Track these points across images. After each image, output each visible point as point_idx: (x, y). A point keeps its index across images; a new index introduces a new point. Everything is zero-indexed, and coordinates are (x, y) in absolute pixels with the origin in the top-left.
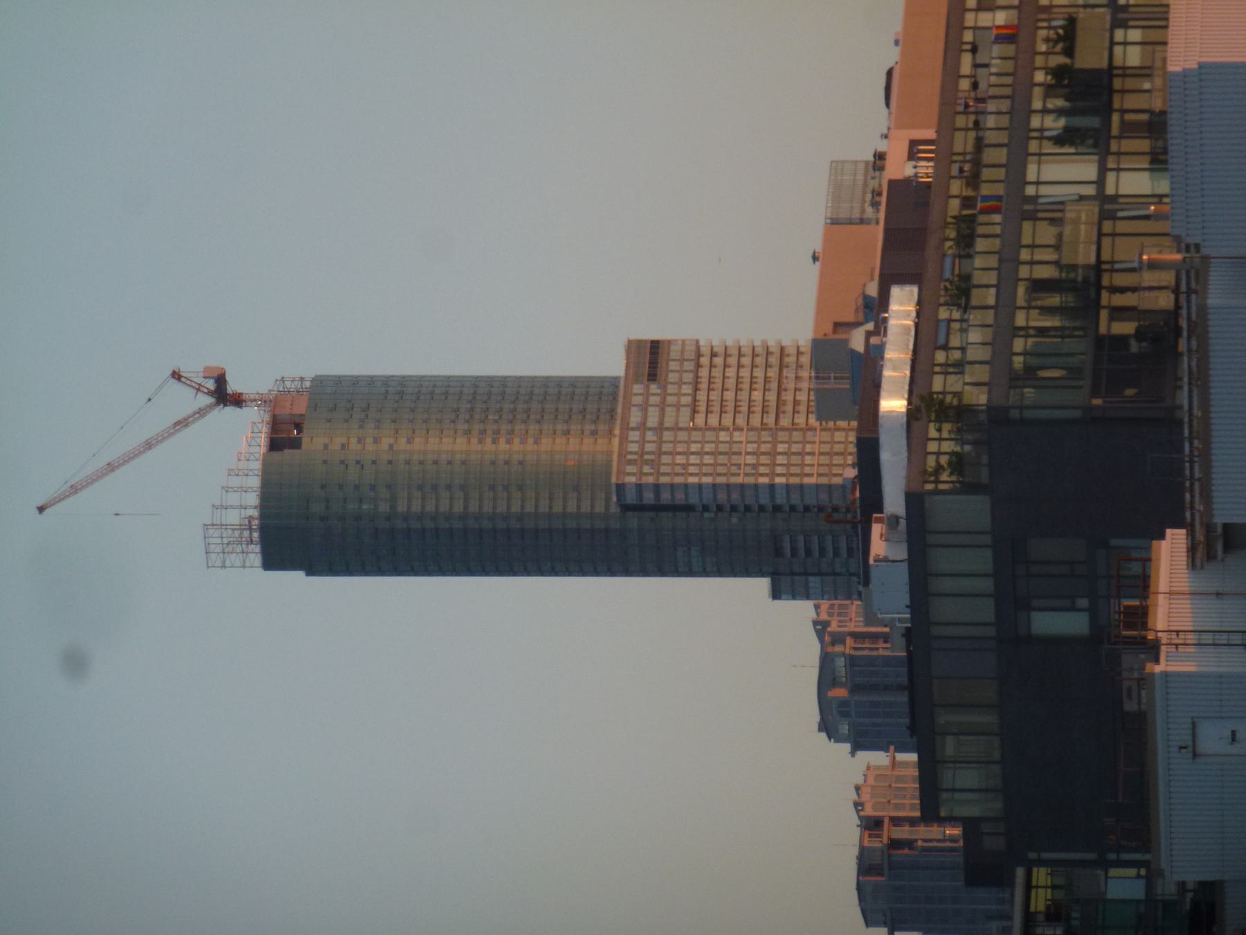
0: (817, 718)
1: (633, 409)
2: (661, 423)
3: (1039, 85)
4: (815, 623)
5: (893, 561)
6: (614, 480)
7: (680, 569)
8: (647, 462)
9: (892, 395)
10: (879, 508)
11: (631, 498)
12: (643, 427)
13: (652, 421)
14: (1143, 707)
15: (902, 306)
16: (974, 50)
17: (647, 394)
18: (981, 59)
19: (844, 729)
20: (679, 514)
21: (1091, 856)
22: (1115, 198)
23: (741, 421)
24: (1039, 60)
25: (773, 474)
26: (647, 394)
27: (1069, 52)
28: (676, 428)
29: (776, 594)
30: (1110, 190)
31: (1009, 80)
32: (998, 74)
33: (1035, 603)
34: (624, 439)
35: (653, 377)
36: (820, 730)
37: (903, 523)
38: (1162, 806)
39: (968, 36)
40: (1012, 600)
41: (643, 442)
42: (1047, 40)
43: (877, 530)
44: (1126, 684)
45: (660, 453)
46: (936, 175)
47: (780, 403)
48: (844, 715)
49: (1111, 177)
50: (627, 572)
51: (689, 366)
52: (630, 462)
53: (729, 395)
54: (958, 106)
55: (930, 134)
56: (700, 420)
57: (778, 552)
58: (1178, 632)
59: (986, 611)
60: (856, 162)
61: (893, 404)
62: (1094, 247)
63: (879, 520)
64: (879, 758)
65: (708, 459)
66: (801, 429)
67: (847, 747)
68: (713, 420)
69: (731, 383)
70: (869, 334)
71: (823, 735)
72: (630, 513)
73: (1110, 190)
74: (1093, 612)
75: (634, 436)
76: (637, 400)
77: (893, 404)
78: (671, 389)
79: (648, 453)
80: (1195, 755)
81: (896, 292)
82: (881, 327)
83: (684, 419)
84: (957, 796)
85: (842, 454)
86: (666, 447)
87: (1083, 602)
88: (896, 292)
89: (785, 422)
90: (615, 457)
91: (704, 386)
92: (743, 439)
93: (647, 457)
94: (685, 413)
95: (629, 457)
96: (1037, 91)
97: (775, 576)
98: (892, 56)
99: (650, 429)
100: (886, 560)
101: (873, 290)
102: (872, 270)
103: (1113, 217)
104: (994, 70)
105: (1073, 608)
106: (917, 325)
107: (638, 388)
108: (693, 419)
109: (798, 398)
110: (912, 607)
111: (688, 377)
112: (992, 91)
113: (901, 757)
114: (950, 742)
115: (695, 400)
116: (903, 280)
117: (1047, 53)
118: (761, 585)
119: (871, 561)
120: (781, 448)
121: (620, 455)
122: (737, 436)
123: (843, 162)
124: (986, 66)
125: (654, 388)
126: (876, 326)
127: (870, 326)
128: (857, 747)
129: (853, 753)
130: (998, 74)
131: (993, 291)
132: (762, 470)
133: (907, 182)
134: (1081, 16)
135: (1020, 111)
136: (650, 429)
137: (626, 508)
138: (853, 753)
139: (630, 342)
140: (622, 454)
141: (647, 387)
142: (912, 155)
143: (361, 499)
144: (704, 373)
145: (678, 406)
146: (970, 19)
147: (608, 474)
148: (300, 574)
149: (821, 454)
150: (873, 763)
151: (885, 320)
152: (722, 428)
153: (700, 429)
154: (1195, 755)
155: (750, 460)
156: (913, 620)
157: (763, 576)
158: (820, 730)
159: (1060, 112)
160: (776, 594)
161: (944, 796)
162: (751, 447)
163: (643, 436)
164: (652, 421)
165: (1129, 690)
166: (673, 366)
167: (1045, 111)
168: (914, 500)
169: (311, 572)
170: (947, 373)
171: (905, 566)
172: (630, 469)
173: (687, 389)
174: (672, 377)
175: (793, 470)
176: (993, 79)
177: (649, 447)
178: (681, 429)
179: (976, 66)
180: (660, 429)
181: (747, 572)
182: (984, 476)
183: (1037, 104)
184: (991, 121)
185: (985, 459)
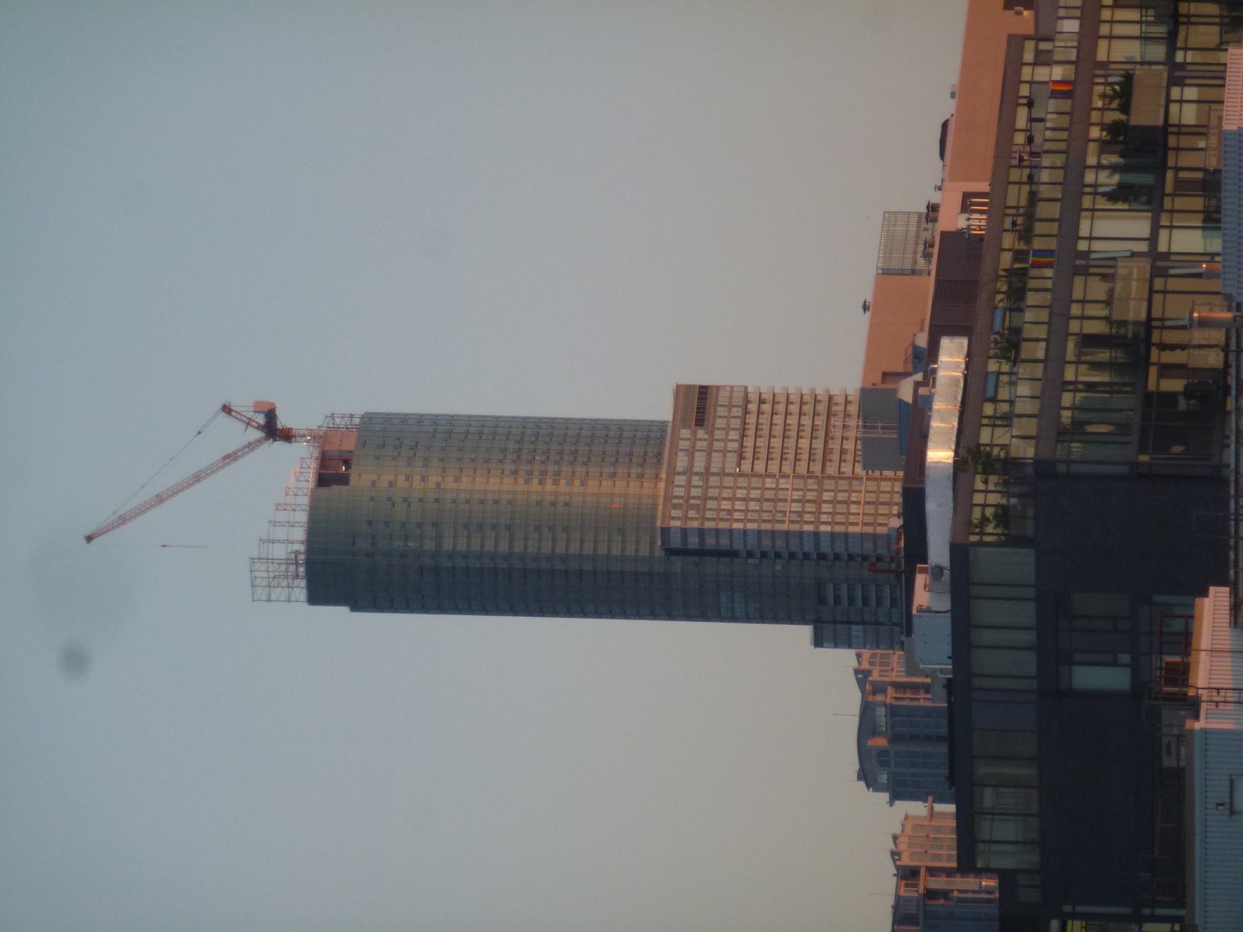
2: (708, 468)
3: (1095, 140)
4: (856, 672)
5: (936, 612)
6: (659, 524)
8: (693, 507)
9: (940, 446)
10: (924, 559)
11: (676, 542)
12: (689, 472)
13: (699, 465)
14: (1182, 763)
15: (952, 357)
16: (1030, 104)
17: (694, 439)
18: (1037, 113)
19: (883, 778)
22: (1167, 256)
24: (1095, 117)
26: (694, 439)
27: (1125, 108)
28: (722, 474)
29: (818, 642)
30: (1162, 247)
31: (1064, 135)
32: (1053, 129)
34: (670, 483)
35: (700, 422)
36: (859, 778)
37: (947, 573)
38: (1197, 862)
39: (1024, 90)
40: (1053, 654)
41: (689, 485)
42: (1103, 96)
43: (921, 580)
44: (1165, 740)
45: (705, 498)
48: (884, 764)
49: (1164, 234)
50: (670, 616)
51: (737, 412)
52: (675, 507)
54: (1015, 159)
55: (984, 187)
56: (746, 466)
57: (822, 600)
58: (1218, 689)
59: (1028, 663)
61: (940, 455)
62: (1145, 304)
63: (924, 571)
64: (917, 808)
65: (753, 506)
66: (848, 478)
67: (885, 796)
68: (760, 467)
69: (778, 430)
70: (917, 385)
71: (862, 784)
72: (674, 558)
73: (1162, 247)
74: (1135, 668)
76: (684, 444)
77: (940, 455)
78: (718, 434)
79: (694, 498)
80: (1232, 812)
81: (946, 343)
82: (930, 378)
83: (731, 466)
84: (994, 847)
86: (712, 493)
88: (946, 343)
89: (832, 470)
90: (661, 501)
91: (751, 432)
92: (789, 486)
93: (692, 502)
94: (732, 459)
95: (675, 501)
96: (1092, 147)
98: (947, 108)
99: (696, 474)
100: (929, 610)
101: (922, 341)
102: (923, 321)
104: (1049, 125)
105: (1115, 664)
106: (966, 377)
107: (685, 433)
108: (739, 465)
110: (955, 658)
111: (736, 423)
112: (1048, 146)
114: (988, 793)
116: (954, 331)
119: (914, 611)
122: (783, 483)
124: (1042, 120)
125: (701, 433)
126: (925, 377)
127: (919, 377)
128: (895, 796)
129: (891, 803)
130: (1053, 129)
131: (1043, 345)
132: (807, 517)
133: (959, 234)
136: (696, 474)
137: (670, 552)
138: (891, 803)
139: (678, 386)
140: (668, 498)
141: (695, 433)
142: (965, 208)
143: (407, 536)
144: (751, 419)
145: (725, 452)
146: (1026, 73)
147: (654, 517)
148: (343, 611)
151: (934, 371)
153: (747, 475)
154: (1232, 812)
155: (796, 507)
156: (954, 671)
157: (805, 622)
158: (859, 778)
159: (1114, 168)
160: (818, 642)
161: (981, 847)
162: (796, 495)
165: (1169, 745)
166: (721, 411)
167: (1099, 167)
168: (958, 551)
169: (355, 607)
171: (949, 615)
172: (675, 513)
173: (734, 435)
174: (720, 423)
175: (839, 518)
176: (1049, 134)
178: (728, 475)
179: (1031, 120)
180: (707, 473)
182: (1030, 530)
183: (1092, 160)
184: (1045, 176)
185: (1030, 513)
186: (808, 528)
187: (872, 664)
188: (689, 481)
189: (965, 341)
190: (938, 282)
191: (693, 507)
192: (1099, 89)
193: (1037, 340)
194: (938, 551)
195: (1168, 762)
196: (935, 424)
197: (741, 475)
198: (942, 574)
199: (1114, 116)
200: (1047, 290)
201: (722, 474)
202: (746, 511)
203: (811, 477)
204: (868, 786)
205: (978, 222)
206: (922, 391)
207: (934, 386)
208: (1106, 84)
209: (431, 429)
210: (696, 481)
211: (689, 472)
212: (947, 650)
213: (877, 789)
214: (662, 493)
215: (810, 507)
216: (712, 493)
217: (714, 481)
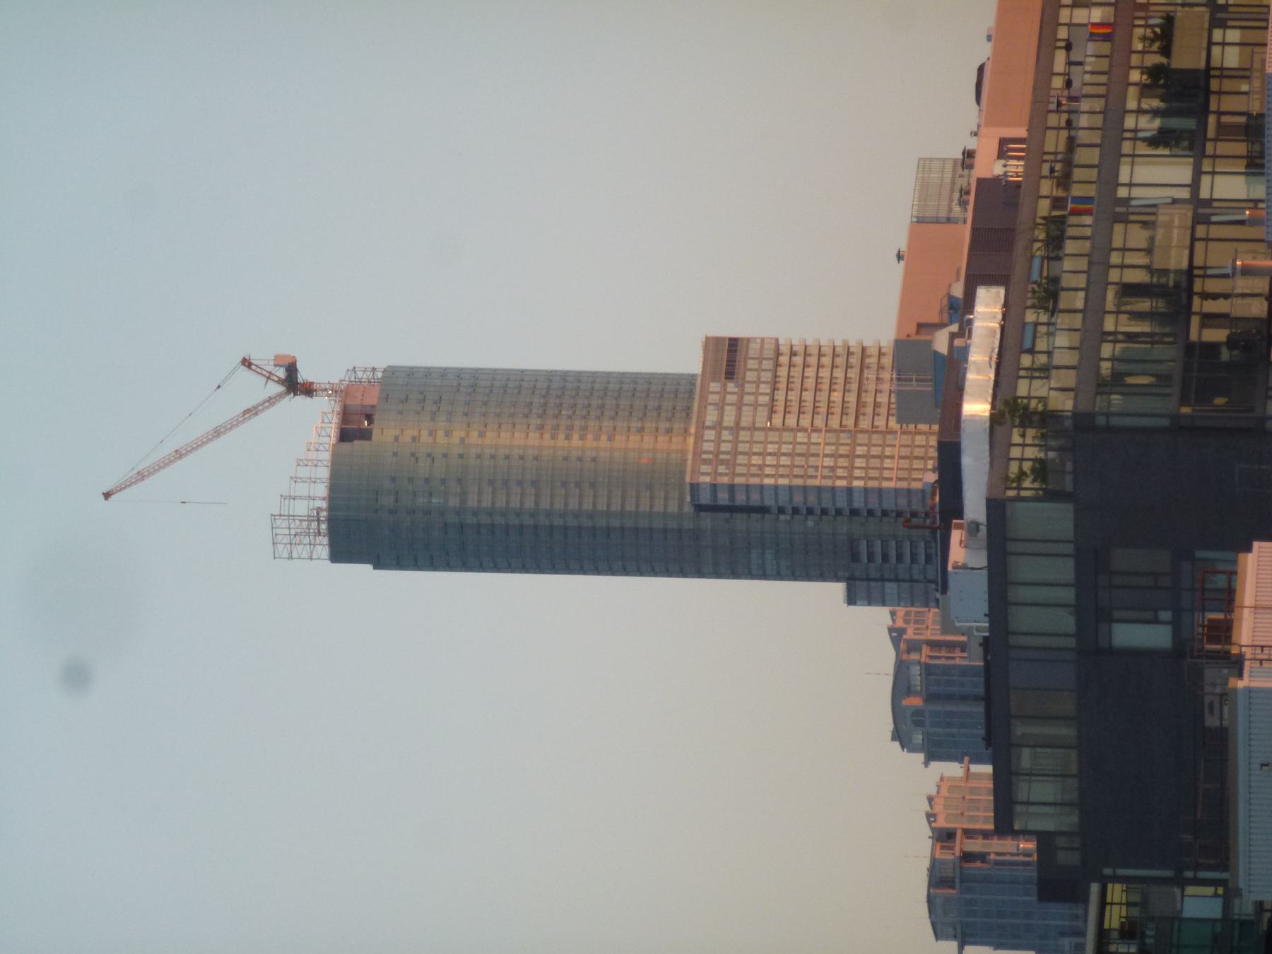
0: (891, 727)
1: (710, 407)
2: (738, 423)
4: (891, 630)
6: (688, 479)
7: (754, 572)
8: (722, 462)
9: (973, 418)
10: (960, 515)
11: (705, 499)
12: (719, 426)
13: (729, 419)
14: (1225, 723)
15: (988, 307)
16: (1068, 47)
17: (724, 392)
18: (1075, 56)
19: (918, 738)
20: (754, 516)
21: (1168, 873)
22: (1211, 200)
23: (819, 422)
24: (1135, 60)
25: (851, 477)
26: (724, 392)
27: (1166, 51)
28: (753, 428)
29: (851, 600)
30: (1204, 194)
31: (1103, 79)
32: (1092, 73)
33: (1116, 614)
34: (699, 438)
35: (730, 375)
36: (893, 739)
37: (983, 529)
39: (1063, 33)
40: (1093, 611)
41: (718, 441)
42: (1144, 39)
43: (956, 536)
45: (735, 453)
46: (1026, 174)
47: (860, 404)
48: (918, 724)
49: (1206, 180)
50: (700, 574)
51: (768, 364)
52: (705, 462)
53: (808, 396)
55: (1022, 132)
56: (777, 420)
57: (855, 557)
59: (1068, 622)
60: (945, 160)
61: (976, 408)
62: (1186, 252)
63: (959, 527)
64: (953, 769)
65: (785, 461)
67: (920, 757)
68: (791, 421)
69: (810, 383)
70: (953, 336)
71: (897, 744)
72: (703, 514)
73: (1204, 194)
74: (1176, 624)
75: (710, 435)
76: (713, 398)
77: (976, 408)
78: (749, 388)
79: (724, 453)
81: (982, 293)
82: (966, 329)
83: (762, 420)
84: (1032, 809)
85: (922, 458)
87: (1166, 615)
88: (982, 293)
89: (865, 424)
90: (690, 456)
92: (820, 440)
93: (722, 457)
94: (762, 413)
95: (704, 456)
96: (1132, 91)
97: (851, 580)
100: (965, 567)
101: (958, 291)
103: (1208, 222)
104: (1088, 68)
105: (1156, 621)
106: (1003, 328)
107: (715, 386)
108: (770, 419)
109: (878, 400)
111: (767, 376)
113: (975, 768)
114: (1026, 753)
115: (773, 400)
116: (990, 281)
117: (1143, 52)
118: (839, 589)
119: (950, 568)
120: (860, 450)
121: (694, 453)
122: (815, 437)
123: (931, 159)
124: (1080, 64)
125: (731, 387)
126: (961, 328)
127: (954, 328)
128: (931, 757)
129: (926, 764)
130: (1092, 73)
131: (1082, 294)
132: (840, 472)
133: (996, 180)
134: (1179, 14)
135: (1113, 115)
137: (699, 508)
138: (926, 764)
140: (697, 453)
141: (725, 386)
142: (1002, 154)
144: (783, 372)
145: (755, 405)
147: (683, 473)
148: (369, 567)
149: (902, 457)
150: (947, 774)
151: (970, 322)
152: (799, 429)
153: (778, 430)
155: (828, 462)
157: (837, 579)
158: (893, 739)
159: (1155, 113)
160: (851, 600)
162: (829, 450)
163: (719, 435)
164: (729, 419)
165: (1211, 705)
166: (751, 364)
167: (1140, 111)
168: (995, 507)
169: (378, 565)
170: (1032, 378)
171: (985, 572)
172: (704, 468)
173: (765, 388)
174: (751, 376)
175: (873, 473)
176: (1088, 78)
177: (725, 447)
179: (1070, 63)
180: (737, 428)
181: (822, 577)
182: (1069, 486)
183: (1132, 104)
184: (1084, 121)
185: (1069, 467)
186: (840, 483)
187: (907, 622)
188: (719, 435)
189: (1001, 291)
190: (974, 230)
191: (722, 462)
192: (1139, 32)
193: (1076, 289)
194: (974, 506)
195: (1211, 721)
196: (971, 376)
197: (772, 429)
198: (978, 530)
199: (1154, 59)
200: (1086, 238)
201: (753, 428)
202: (777, 466)
203: (844, 431)
204: (903, 747)
205: (1015, 168)
206: (958, 342)
207: (970, 337)
208: (1146, 26)
209: (455, 383)
210: (726, 435)
211: (719, 426)
212: (984, 607)
213: (912, 749)
214: (691, 448)
215: (843, 462)
216: (742, 447)
217: (744, 435)
